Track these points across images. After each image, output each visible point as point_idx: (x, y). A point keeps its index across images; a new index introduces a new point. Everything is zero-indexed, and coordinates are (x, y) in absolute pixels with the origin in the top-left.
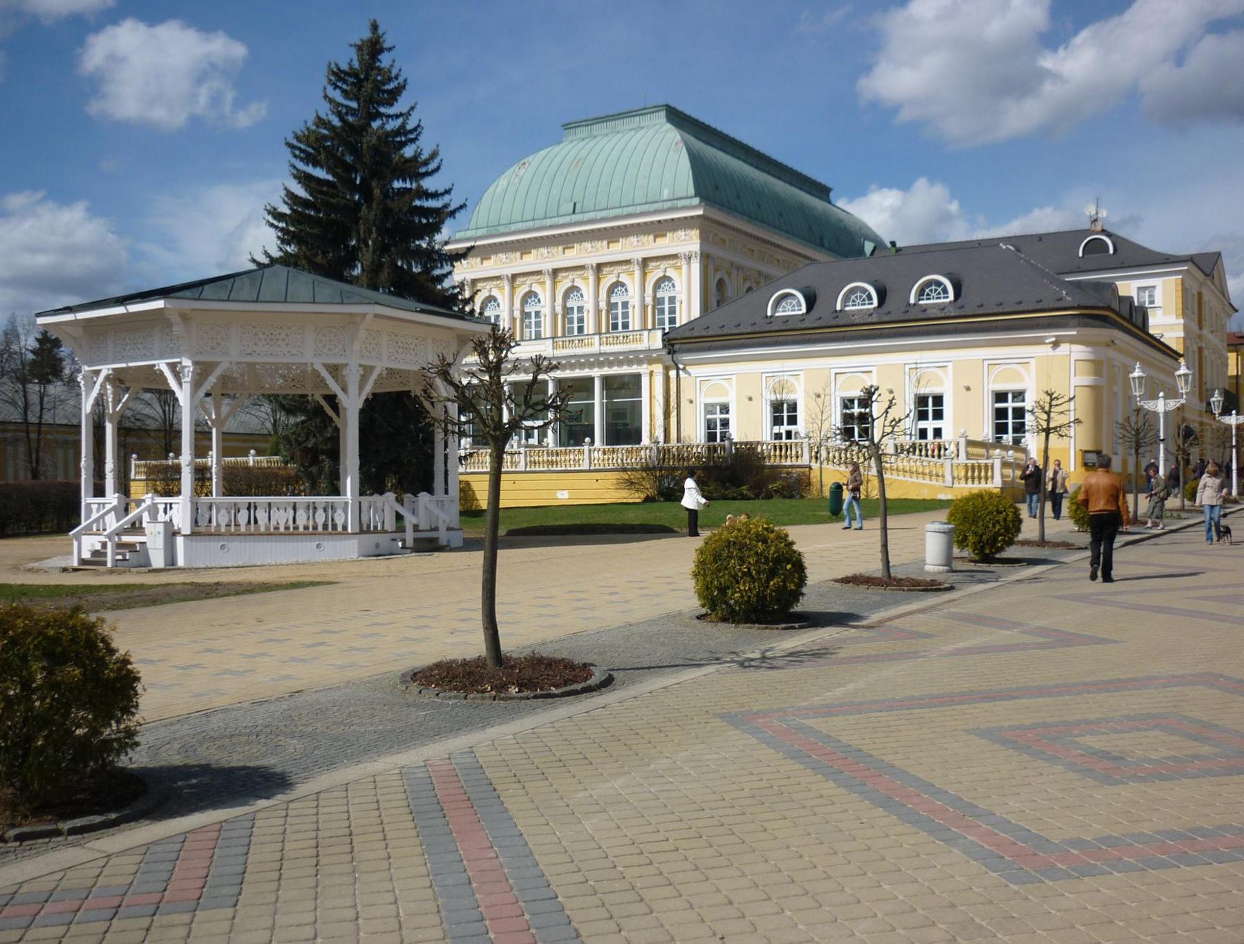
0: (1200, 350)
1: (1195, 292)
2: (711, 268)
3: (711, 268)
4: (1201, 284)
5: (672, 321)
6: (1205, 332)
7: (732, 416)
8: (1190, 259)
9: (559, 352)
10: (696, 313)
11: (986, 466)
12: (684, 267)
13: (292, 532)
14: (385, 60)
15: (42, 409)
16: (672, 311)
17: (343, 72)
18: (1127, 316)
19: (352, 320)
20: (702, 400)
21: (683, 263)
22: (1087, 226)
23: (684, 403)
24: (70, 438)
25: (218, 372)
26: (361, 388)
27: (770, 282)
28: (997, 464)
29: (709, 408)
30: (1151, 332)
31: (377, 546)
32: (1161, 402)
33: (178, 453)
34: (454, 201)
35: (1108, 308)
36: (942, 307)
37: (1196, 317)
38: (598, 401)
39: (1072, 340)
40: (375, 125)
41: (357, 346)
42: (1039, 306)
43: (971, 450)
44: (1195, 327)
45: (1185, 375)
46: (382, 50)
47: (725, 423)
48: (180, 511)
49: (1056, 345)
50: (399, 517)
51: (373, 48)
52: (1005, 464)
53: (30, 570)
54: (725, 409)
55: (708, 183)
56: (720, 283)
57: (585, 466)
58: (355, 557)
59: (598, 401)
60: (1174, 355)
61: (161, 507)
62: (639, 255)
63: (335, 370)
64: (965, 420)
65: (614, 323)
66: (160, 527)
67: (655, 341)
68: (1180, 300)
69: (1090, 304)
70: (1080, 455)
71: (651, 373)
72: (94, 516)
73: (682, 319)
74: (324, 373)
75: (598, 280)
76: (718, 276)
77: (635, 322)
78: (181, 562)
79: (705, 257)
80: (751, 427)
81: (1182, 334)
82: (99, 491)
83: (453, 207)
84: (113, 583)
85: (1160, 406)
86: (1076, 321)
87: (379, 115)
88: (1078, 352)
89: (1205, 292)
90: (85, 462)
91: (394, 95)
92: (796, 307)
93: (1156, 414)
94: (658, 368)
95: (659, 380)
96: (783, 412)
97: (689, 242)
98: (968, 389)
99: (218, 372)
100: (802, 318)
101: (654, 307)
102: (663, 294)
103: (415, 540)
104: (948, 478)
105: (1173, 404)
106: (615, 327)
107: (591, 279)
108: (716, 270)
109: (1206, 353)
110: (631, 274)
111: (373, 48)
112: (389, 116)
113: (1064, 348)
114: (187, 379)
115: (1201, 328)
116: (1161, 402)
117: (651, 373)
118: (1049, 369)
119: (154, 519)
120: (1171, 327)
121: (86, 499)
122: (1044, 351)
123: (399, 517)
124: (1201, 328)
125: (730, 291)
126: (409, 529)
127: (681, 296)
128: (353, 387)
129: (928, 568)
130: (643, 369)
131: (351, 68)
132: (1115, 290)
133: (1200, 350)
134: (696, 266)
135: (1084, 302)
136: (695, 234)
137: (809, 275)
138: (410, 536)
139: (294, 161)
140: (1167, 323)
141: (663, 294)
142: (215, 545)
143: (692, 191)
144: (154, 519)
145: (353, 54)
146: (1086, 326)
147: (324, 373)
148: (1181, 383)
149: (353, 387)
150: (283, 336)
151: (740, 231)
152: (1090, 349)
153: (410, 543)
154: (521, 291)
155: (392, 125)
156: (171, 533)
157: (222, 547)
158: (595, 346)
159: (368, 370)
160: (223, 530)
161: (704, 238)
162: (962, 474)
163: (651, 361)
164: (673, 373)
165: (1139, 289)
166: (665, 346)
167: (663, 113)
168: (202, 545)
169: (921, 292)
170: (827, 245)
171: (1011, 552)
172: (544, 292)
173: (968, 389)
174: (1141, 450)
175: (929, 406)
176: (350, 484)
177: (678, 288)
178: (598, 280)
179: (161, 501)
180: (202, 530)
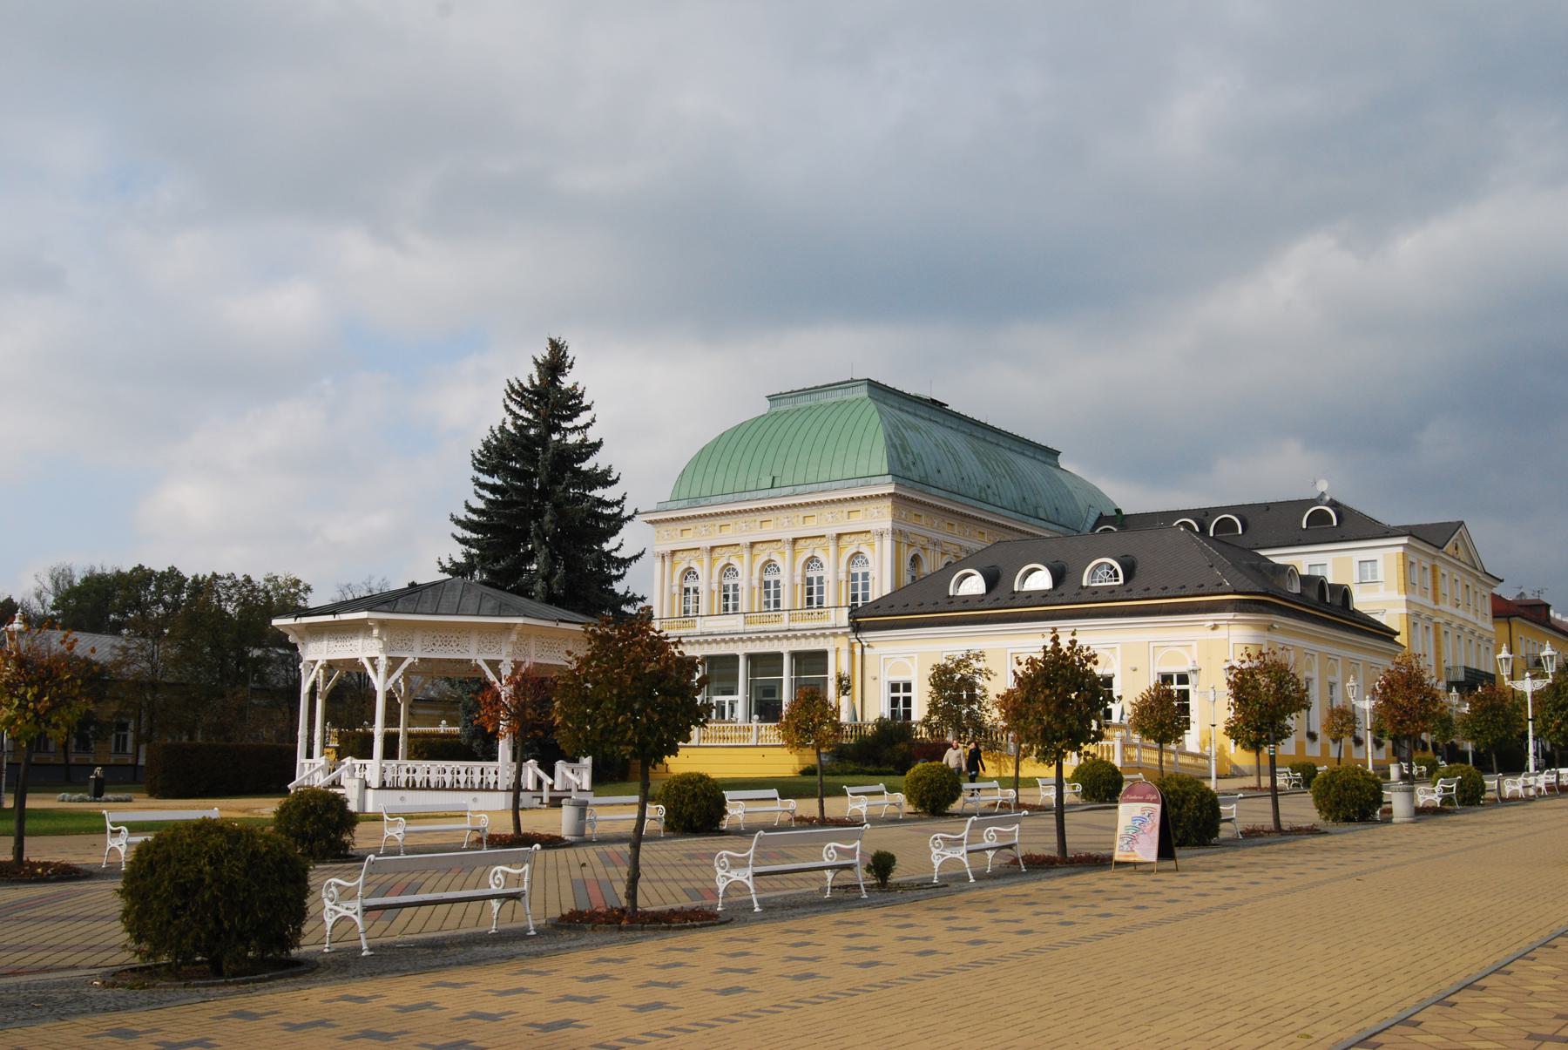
5: (865, 597)
8: (1410, 532)
9: (750, 628)
12: (877, 544)
14: (566, 382)
16: (866, 587)
19: (508, 628)
21: (877, 538)
25: (405, 665)
33: (372, 722)
36: (1112, 590)
37: (1430, 592)
38: (786, 677)
40: (556, 437)
42: (1201, 591)
47: (907, 701)
49: (1215, 627)
50: (540, 782)
51: (555, 365)
54: (908, 687)
57: (753, 742)
59: (786, 677)
62: (745, 540)
63: (494, 665)
65: (812, 596)
66: (356, 782)
67: (843, 617)
72: (307, 773)
73: (874, 596)
74: (485, 667)
76: (912, 552)
77: (829, 600)
79: (897, 534)
81: (1404, 611)
82: (310, 755)
85: (1527, 686)
87: (557, 428)
90: (302, 732)
91: (576, 411)
93: (1524, 694)
94: (843, 644)
97: (881, 518)
99: (405, 665)
103: (551, 798)
105: (1540, 684)
110: (826, 550)
111: (555, 365)
112: (566, 429)
113: (1222, 632)
114: (382, 669)
118: (1207, 649)
119: (353, 776)
121: (301, 759)
123: (540, 782)
126: (545, 788)
127: (873, 573)
131: (455, 564)
134: (888, 543)
136: (887, 505)
138: (546, 794)
139: (508, 402)
144: (353, 776)
147: (485, 667)
153: (546, 800)
158: (785, 622)
161: (896, 519)
164: (858, 650)
166: (851, 625)
169: (1093, 574)
171: (956, 807)
176: (504, 748)
179: (358, 762)
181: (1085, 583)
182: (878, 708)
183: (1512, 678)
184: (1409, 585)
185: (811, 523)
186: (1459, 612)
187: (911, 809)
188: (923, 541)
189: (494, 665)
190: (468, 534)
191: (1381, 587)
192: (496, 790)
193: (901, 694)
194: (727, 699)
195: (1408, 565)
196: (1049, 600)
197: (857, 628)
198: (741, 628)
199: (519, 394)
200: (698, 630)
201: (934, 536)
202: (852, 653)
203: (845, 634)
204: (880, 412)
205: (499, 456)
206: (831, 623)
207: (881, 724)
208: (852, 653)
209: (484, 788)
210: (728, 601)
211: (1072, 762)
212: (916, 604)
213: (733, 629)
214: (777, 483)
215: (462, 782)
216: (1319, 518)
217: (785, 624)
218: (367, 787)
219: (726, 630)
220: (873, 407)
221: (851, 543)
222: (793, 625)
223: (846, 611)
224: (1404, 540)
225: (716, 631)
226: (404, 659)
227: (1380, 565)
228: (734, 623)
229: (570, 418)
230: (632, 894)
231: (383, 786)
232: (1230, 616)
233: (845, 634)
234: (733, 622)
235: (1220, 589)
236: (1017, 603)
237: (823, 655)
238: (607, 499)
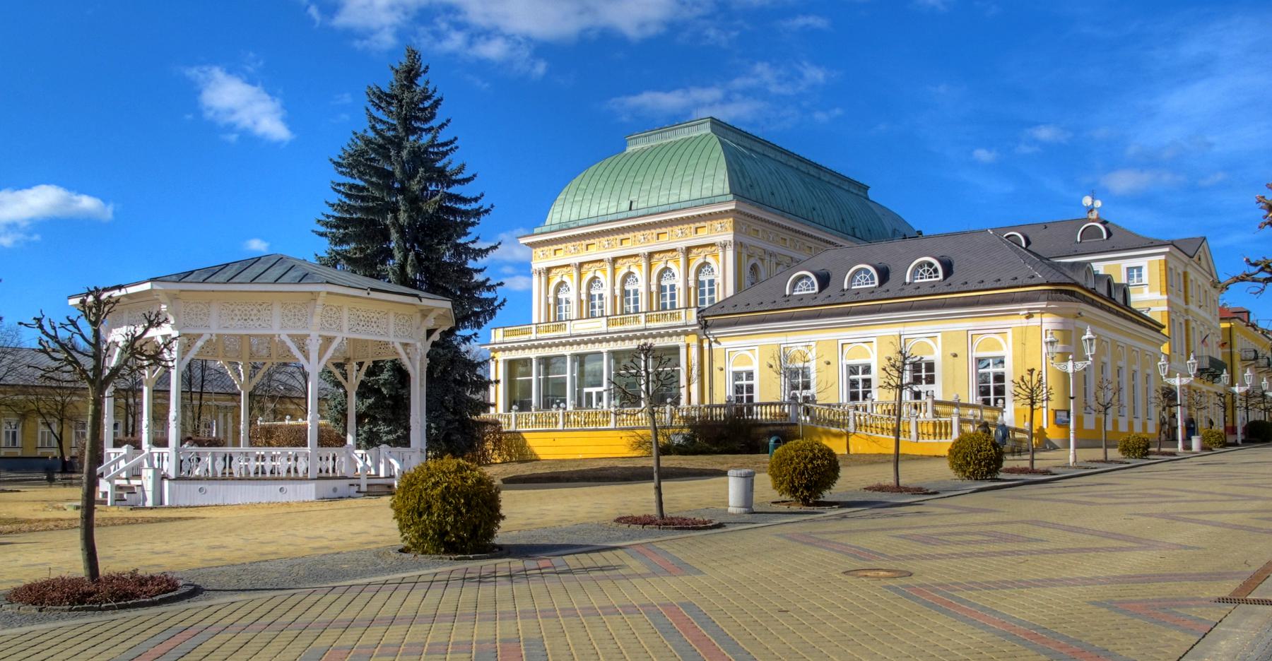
0: (1187, 321)
1: (1180, 271)
2: (744, 257)
3: (744, 257)
4: (1186, 265)
6: (1192, 307)
7: (756, 382)
8: (1172, 244)
9: (612, 329)
10: (730, 292)
11: (946, 423)
12: (721, 254)
13: (260, 476)
15: (203, 381)
16: (711, 292)
17: (387, 95)
18: (1105, 293)
20: (731, 368)
22: (1084, 215)
23: (716, 372)
24: (164, 402)
26: (320, 359)
27: (794, 264)
28: (955, 419)
29: (737, 375)
30: (1133, 306)
31: (335, 490)
32: (1070, 364)
34: (484, 203)
35: (1076, 284)
36: (933, 285)
37: (1182, 294)
39: (1043, 311)
41: (317, 320)
42: (1015, 283)
43: (939, 408)
44: (1181, 302)
45: (1090, 339)
46: (417, 75)
48: (169, 459)
49: (1029, 316)
52: (962, 421)
53: (58, 508)
54: (750, 375)
55: (741, 187)
56: (754, 268)
58: (313, 498)
60: (1155, 327)
61: (156, 456)
64: (954, 383)
67: (693, 316)
68: (1164, 278)
69: (1058, 281)
70: (1051, 414)
71: (688, 346)
73: (719, 297)
75: (650, 267)
76: (752, 261)
77: (680, 301)
78: (166, 503)
79: (738, 245)
80: (769, 392)
81: (1166, 308)
83: (486, 207)
84: (887, 520)
86: (1045, 296)
87: (414, 131)
88: (1048, 322)
89: (1189, 270)
92: (810, 287)
94: (693, 340)
95: (694, 352)
96: (797, 377)
97: (723, 233)
98: (955, 356)
100: (814, 297)
101: (696, 289)
102: (704, 278)
104: (913, 433)
105: (1080, 365)
106: (664, 308)
107: (644, 265)
108: (749, 256)
109: (1193, 324)
113: (1036, 320)
115: (1187, 303)
116: (1070, 364)
117: (688, 346)
118: (1020, 340)
120: (1157, 302)
122: (1018, 322)
124: (1187, 303)
125: (763, 275)
127: (719, 280)
128: (314, 356)
129: (731, 510)
130: (679, 341)
132: (1090, 269)
133: (1187, 321)
134: (730, 253)
135: (1052, 280)
136: (728, 223)
137: (824, 260)
140: (1149, 296)
141: (704, 278)
142: (195, 486)
143: (727, 190)
145: (392, 77)
146: (1054, 300)
148: (1086, 346)
149: (314, 356)
150: (255, 311)
151: (768, 222)
152: (1060, 319)
153: (364, 488)
154: (587, 277)
155: (426, 139)
156: (161, 477)
157: (281, 490)
159: (328, 340)
160: (252, 475)
161: (737, 231)
162: (931, 431)
163: (686, 333)
164: (706, 345)
165: (1128, 269)
166: (699, 323)
167: (708, 124)
168: (184, 486)
170: (858, 234)
171: (827, 495)
172: (605, 278)
173: (955, 356)
174: (1036, 406)
175: (924, 372)
177: (716, 272)
178: (650, 267)
180: (301, 475)
181: (908, 280)
182: (723, 392)
183: (1168, 376)
184: (1168, 288)
185: (663, 238)
186: (1201, 312)
187: (775, 495)
188: (760, 252)
189: (301, 341)
190: (323, 229)
191: (1146, 289)
192: (305, 479)
193: (745, 382)
194: (594, 390)
195: (1168, 270)
196: (875, 296)
197: (704, 325)
198: (604, 329)
199: (382, 98)
200: (567, 332)
201: (771, 248)
202: (701, 349)
203: (694, 332)
204: (723, 144)
205: (365, 161)
206: (682, 322)
207: (728, 405)
208: (701, 349)
209: (293, 477)
210: (589, 307)
211: (956, 435)
212: (755, 303)
213: (598, 330)
214: (634, 207)
215: (301, 469)
216: (1091, 233)
217: (642, 325)
218: (164, 477)
219: (592, 331)
220: (715, 139)
221: (698, 255)
222: (649, 325)
223: (694, 311)
224: (1167, 249)
225: (583, 332)
226: (200, 336)
227: (1145, 272)
228: (599, 325)
229: (426, 120)
230: (658, 489)
231: (178, 479)
232: (1043, 305)
233: (694, 332)
234: (598, 325)
235: (1033, 281)
236: (847, 299)
237: (676, 350)
238: (465, 195)
